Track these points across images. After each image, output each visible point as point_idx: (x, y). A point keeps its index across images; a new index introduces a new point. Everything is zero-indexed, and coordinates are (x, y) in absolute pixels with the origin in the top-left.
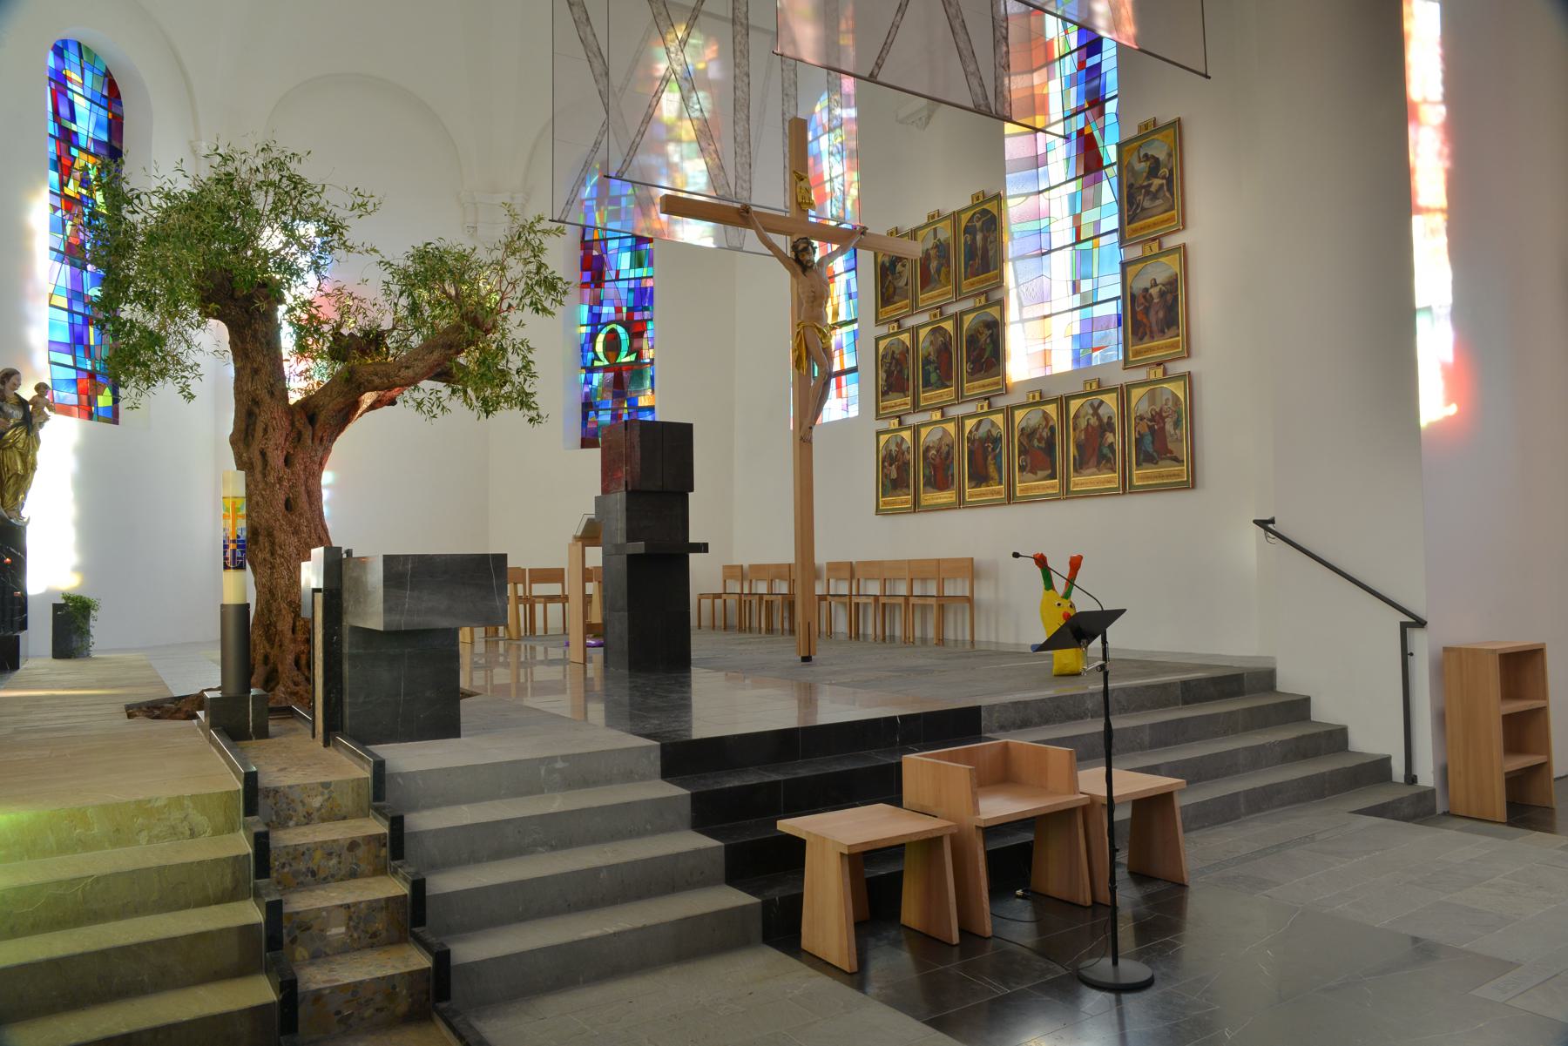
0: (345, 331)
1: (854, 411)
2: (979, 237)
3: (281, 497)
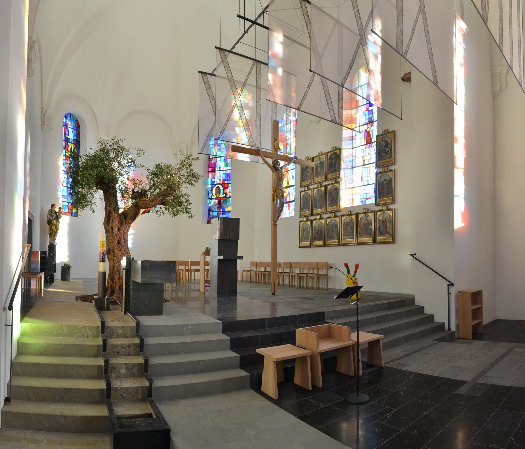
0: (136, 191)
1: (293, 214)
2: (333, 161)
3: (117, 240)
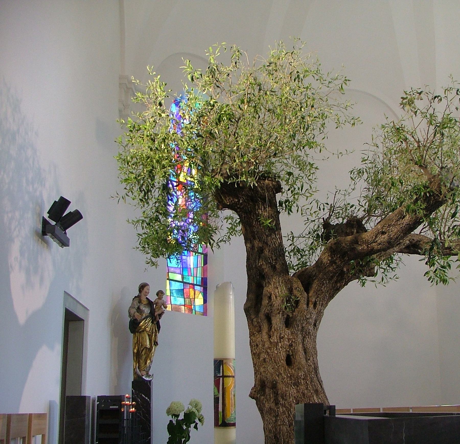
3: (283, 355)
